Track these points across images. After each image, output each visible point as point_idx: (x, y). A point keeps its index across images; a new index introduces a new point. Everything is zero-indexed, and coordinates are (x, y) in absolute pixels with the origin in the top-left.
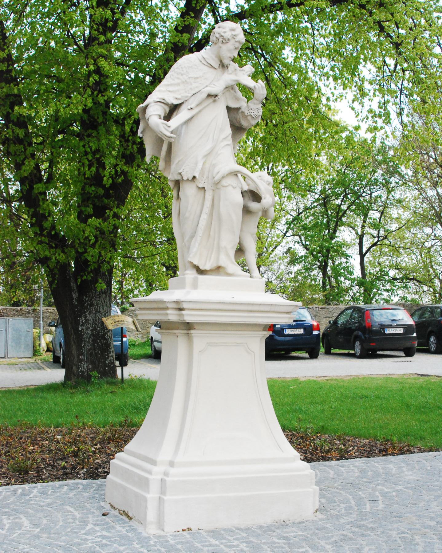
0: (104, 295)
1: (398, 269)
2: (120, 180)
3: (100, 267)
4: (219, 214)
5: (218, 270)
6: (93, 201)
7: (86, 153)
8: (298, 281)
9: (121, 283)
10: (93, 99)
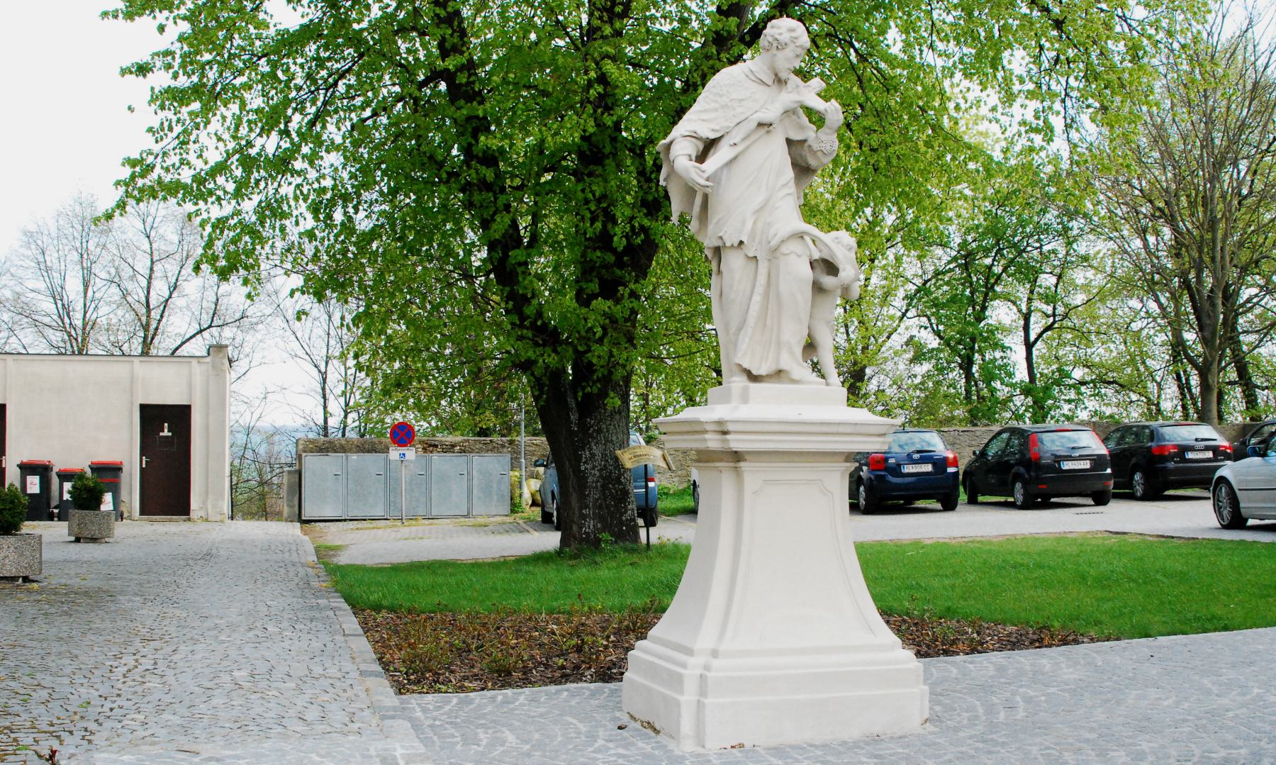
0: (617, 417)
1: (1088, 367)
2: (639, 241)
3: (610, 373)
4: (778, 295)
5: (779, 375)
6: (599, 273)
7: (587, 202)
8: (926, 389)
9: (645, 398)
10: (596, 120)
